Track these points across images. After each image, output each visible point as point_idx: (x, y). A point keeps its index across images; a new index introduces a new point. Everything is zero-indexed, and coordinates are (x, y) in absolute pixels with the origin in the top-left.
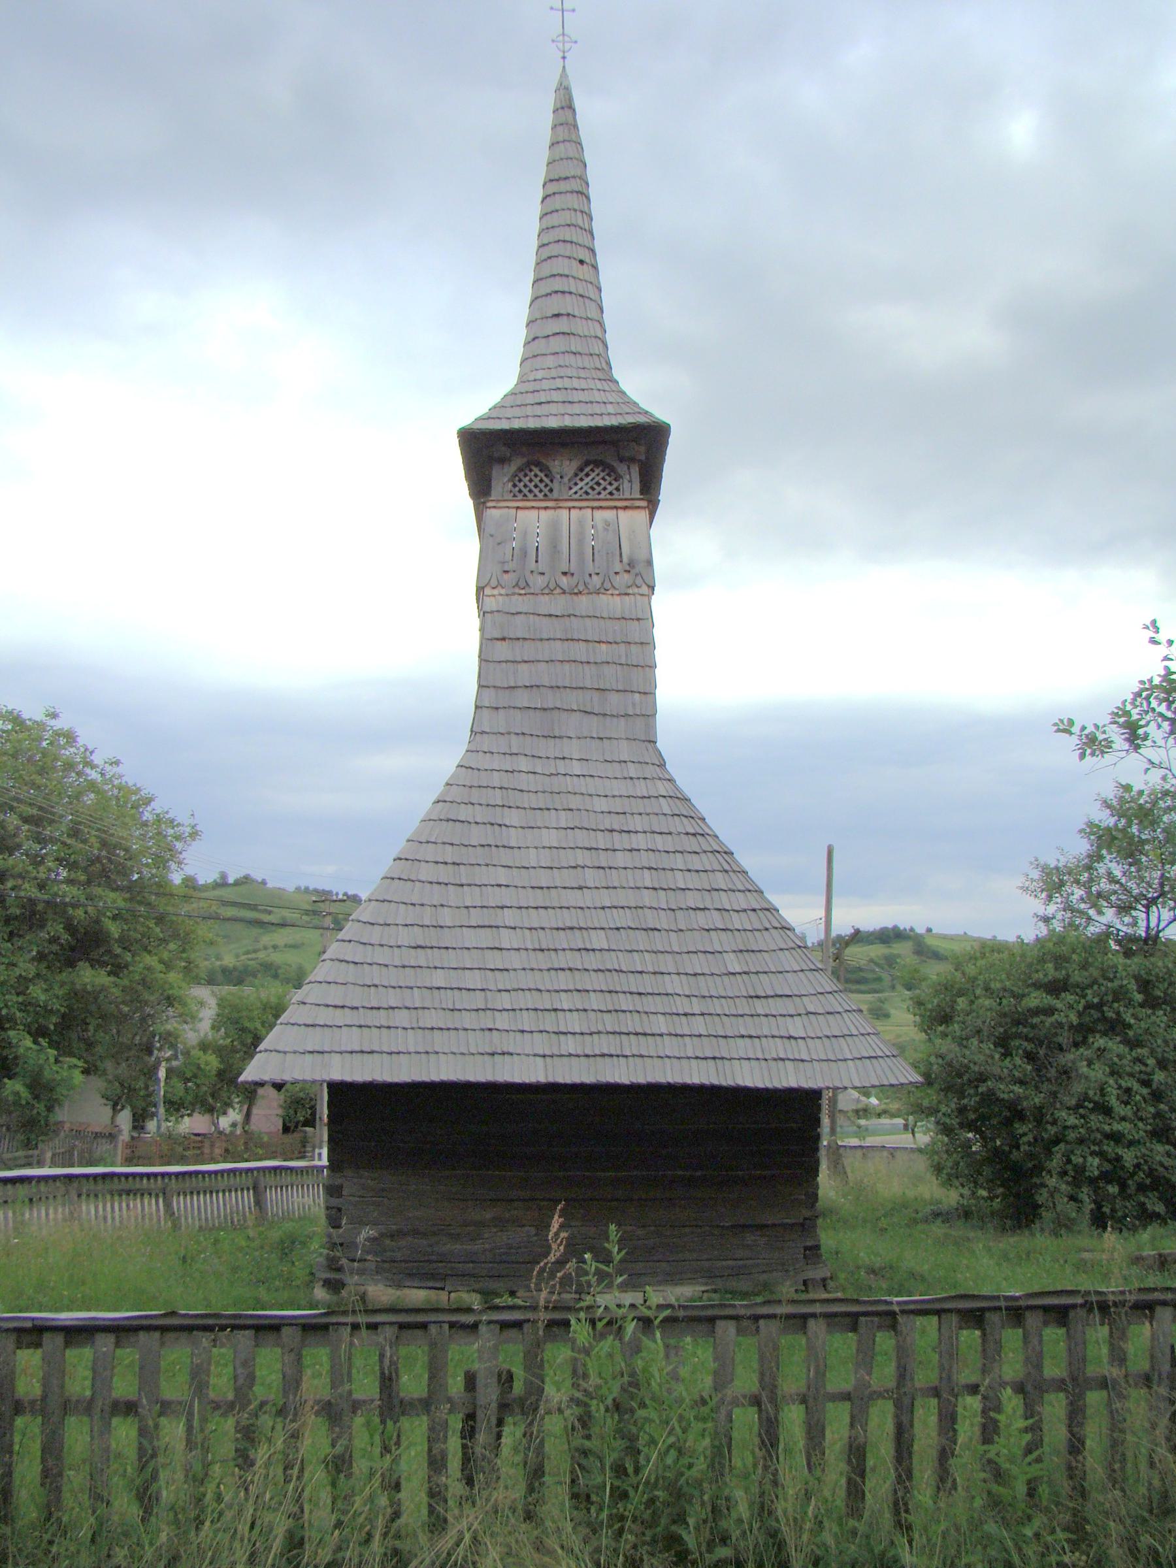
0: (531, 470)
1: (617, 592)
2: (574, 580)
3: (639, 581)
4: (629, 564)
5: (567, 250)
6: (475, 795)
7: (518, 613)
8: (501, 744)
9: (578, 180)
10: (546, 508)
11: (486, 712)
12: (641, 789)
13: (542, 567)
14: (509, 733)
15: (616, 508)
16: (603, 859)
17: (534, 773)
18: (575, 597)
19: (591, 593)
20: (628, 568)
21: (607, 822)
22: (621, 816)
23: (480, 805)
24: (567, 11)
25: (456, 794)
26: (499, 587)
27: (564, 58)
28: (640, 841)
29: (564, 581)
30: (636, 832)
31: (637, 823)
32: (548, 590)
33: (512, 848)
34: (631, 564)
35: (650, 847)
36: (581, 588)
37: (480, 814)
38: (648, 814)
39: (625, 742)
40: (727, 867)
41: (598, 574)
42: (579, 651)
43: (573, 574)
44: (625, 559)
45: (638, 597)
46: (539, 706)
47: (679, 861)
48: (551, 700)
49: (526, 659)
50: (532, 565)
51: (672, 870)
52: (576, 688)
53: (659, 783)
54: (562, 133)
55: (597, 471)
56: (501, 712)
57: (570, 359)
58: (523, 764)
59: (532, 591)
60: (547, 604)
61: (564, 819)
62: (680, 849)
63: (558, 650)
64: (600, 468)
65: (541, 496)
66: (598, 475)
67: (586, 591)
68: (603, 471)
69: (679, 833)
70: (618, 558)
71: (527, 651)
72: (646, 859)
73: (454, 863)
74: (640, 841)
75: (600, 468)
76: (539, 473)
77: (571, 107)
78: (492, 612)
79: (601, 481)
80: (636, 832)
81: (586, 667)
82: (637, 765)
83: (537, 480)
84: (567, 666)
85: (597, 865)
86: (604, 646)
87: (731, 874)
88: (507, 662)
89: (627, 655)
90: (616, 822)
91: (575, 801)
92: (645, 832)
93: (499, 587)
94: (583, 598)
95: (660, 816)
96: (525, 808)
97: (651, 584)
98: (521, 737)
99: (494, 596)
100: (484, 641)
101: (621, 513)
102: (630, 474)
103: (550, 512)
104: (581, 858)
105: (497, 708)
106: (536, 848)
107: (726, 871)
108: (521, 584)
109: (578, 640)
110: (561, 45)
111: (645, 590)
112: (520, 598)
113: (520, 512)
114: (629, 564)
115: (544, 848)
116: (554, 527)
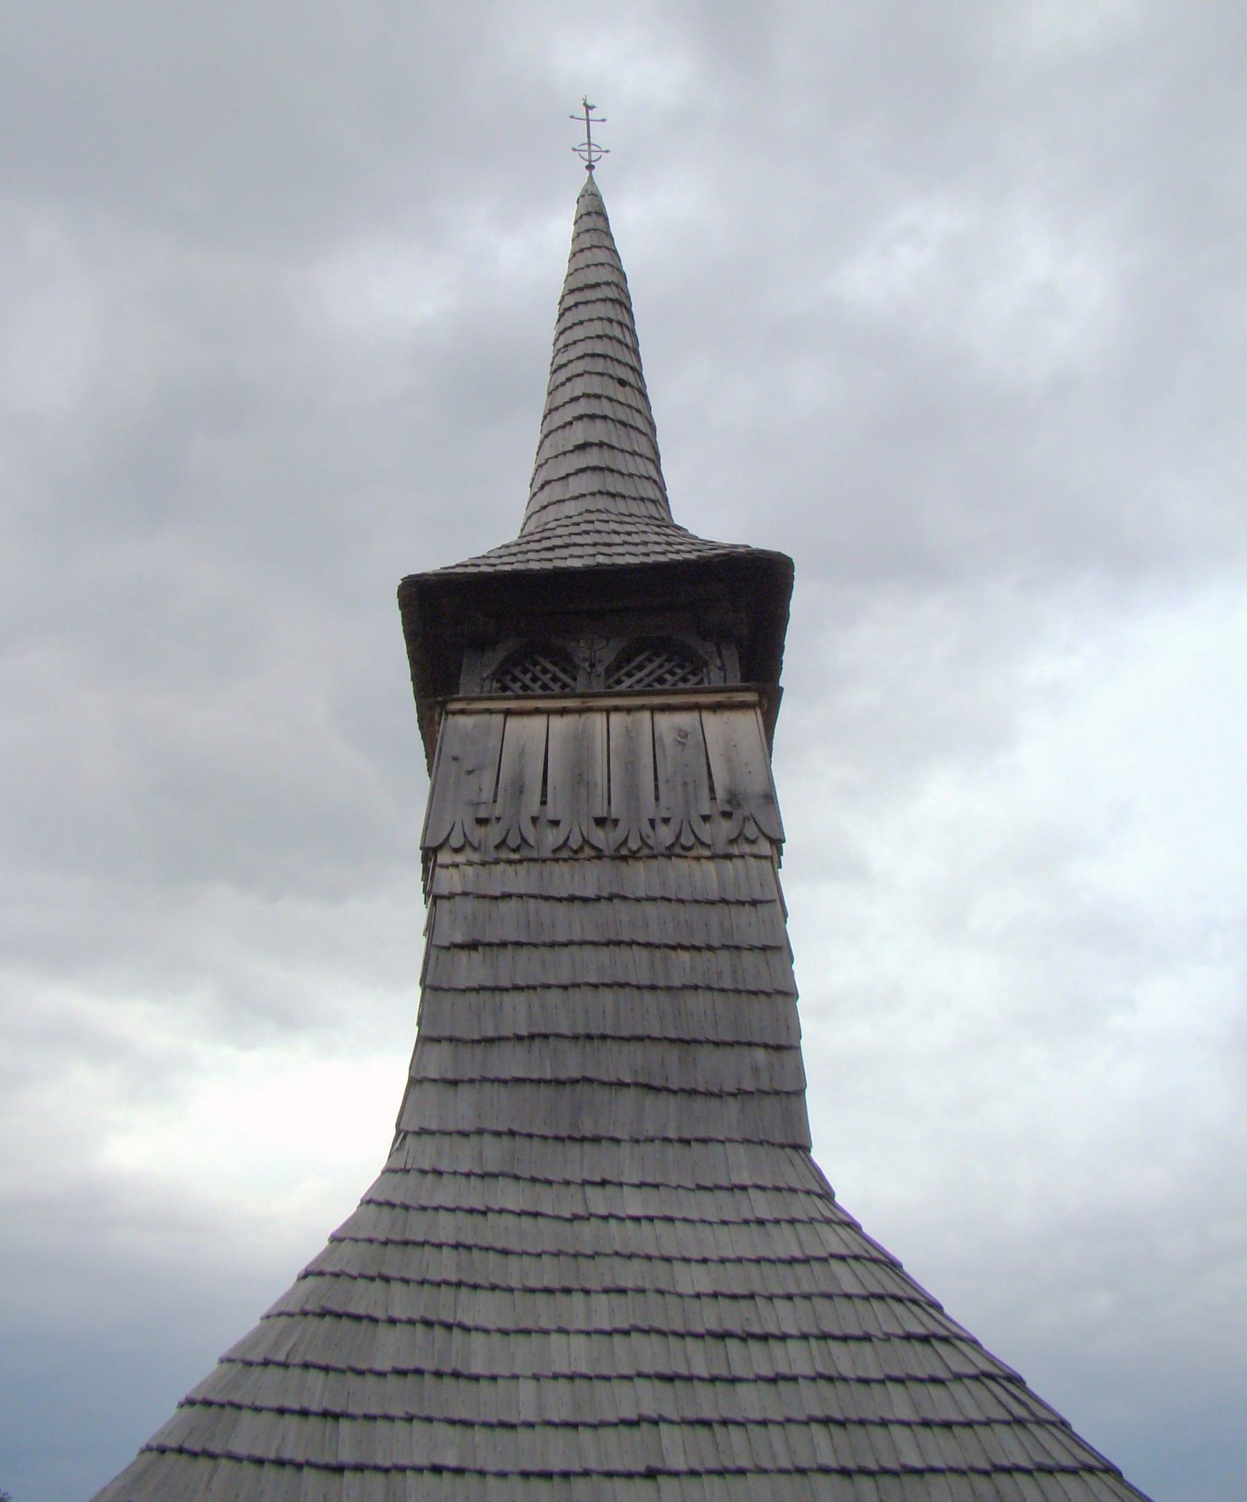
0: (536, 663)
1: (707, 853)
2: (617, 835)
3: (751, 831)
4: (729, 802)
5: (600, 365)
6: (394, 1262)
7: (506, 896)
8: (465, 1156)
9: (614, 288)
10: (563, 712)
11: (431, 1090)
12: (784, 1243)
13: (551, 812)
14: (480, 1132)
15: (698, 707)
16: (707, 1402)
17: (536, 1215)
18: (623, 865)
19: (654, 857)
20: (728, 808)
21: (709, 1317)
22: (744, 1304)
23: (406, 1281)
24: (592, 120)
25: (351, 1259)
26: (468, 850)
27: (590, 167)
28: (795, 1358)
29: (599, 837)
30: (784, 1337)
31: (786, 1318)
32: (567, 853)
33: (476, 1378)
34: (734, 799)
35: (821, 1369)
36: (634, 844)
37: (402, 1302)
38: (808, 1297)
39: (741, 1150)
40: (1020, 1412)
41: (666, 821)
42: (636, 965)
43: (616, 822)
44: (720, 793)
45: (752, 861)
46: (549, 1076)
47: (899, 1404)
48: (572, 1063)
49: (521, 983)
50: (532, 803)
51: (884, 1423)
52: (628, 1039)
53: (825, 1230)
54: (589, 222)
55: (657, 662)
56: (464, 1090)
57: (601, 503)
58: (511, 1196)
59: (535, 855)
60: (563, 879)
61: (605, 1312)
62: (898, 1372)
63: (592, 964)
64: (664, 657)
65: (556, 688)
66: (660, 666)
67: (646, 851)
68: (668, 660)
69: (888, 1337)
70: (705, 792)
71: (526, 967)
72: (812, 1400)
73: (325, 1414)
74: (795, 1358)
75: (664, 657)
76: (549, 666)
77: (601, 214)
78: (451, 897)
79: (668, 677)
80: (784, 1337)
81: (648, 996)
82: (770, 1194)
83: (546, 678)
84: (607, 996)
85: (691, 1414)
86: (685, 956)
87: (1033, 1428)
88: (477, 990)
89: (735, 972)
90: (732, 1317)
91: (629, 1274)
92: (805, 1337)
93: (468, 850)
94: (640, 867)
95: (838, 1301)
96: (511, 1290)
97: (775, 836)
98: (506, 1140)
99: (456, 866)
100: (434, 952)
101: (708, 717)
102: (720, 657)
103: (569, 720)
104: (649, 1398)
105: (455, 1083)
106: (536, 1377)
107: (1020, 1422)
108: (513, 841)
109: (631, 944)
110: (586, 155)
111: (765, 848)
112: (510, 869)
113: (513, 723)
114: (729, 802)
115: (556, 1377)
116: (580, 746)
